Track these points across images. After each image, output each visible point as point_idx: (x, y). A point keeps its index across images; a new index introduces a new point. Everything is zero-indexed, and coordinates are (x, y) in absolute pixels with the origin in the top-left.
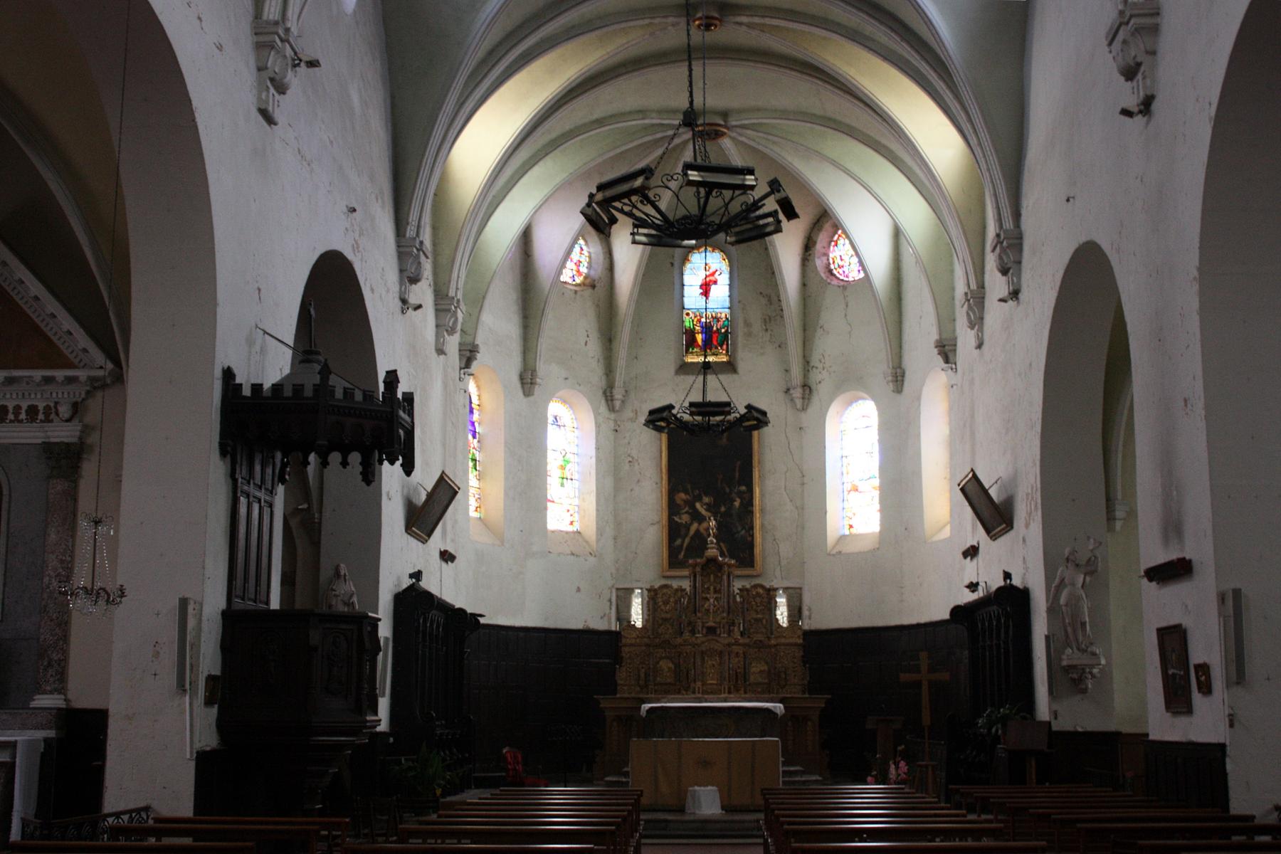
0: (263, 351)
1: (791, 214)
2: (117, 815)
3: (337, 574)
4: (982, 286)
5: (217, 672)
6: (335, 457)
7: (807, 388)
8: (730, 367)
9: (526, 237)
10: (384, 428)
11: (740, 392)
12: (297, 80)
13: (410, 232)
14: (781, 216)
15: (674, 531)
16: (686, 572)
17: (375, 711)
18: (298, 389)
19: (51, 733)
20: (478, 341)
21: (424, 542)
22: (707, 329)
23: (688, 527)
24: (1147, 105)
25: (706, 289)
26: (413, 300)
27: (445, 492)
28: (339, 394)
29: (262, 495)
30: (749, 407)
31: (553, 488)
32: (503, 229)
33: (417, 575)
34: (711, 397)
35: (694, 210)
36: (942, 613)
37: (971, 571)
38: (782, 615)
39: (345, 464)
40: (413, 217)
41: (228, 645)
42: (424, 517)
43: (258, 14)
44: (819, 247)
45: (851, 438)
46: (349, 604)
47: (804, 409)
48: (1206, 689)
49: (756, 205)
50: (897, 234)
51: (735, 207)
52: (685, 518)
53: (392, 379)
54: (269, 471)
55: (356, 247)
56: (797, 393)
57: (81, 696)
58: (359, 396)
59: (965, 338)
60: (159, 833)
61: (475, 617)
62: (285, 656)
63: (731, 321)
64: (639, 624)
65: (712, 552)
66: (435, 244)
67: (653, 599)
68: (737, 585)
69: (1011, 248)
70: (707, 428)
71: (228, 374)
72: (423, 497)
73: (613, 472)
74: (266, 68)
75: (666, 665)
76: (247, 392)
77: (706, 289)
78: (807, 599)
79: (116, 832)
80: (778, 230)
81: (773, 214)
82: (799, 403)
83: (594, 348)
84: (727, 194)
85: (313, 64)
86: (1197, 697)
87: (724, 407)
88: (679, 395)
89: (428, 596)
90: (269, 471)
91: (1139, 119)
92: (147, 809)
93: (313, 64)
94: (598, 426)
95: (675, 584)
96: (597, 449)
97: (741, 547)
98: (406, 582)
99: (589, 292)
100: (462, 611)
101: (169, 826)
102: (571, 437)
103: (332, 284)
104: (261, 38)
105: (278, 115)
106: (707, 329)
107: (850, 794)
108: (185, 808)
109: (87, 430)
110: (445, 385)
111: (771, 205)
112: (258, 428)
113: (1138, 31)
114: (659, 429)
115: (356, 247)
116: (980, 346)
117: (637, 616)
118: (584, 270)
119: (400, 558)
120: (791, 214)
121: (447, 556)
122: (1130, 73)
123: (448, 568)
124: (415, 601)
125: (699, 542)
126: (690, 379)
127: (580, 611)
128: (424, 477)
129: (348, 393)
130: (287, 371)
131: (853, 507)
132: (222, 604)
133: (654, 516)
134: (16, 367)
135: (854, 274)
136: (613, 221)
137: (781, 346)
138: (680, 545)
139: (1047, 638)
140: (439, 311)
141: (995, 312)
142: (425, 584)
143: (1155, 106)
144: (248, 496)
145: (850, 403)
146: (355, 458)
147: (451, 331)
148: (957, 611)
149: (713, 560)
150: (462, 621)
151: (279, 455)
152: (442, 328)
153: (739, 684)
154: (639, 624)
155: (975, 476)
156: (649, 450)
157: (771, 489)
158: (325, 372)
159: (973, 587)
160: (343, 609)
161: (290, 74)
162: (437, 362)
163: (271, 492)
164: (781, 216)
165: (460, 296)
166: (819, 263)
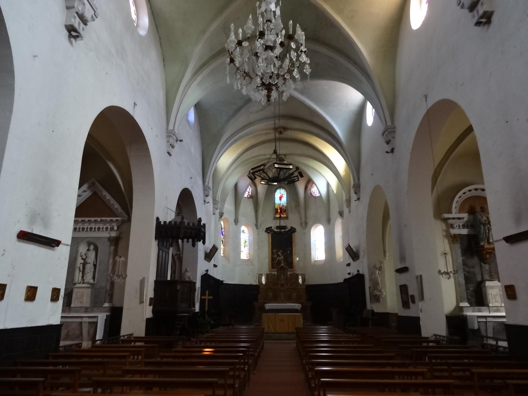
0: (167, 213)
1: (302, 176)
2: (124, 336)
3: (186, 270)
4: (350, 197)
5: (152, 296)
6: (185, 240)
7: (306, 223)
8: (287, 218)
9: (236, 186)
10: (197, 233)
11: (289, 224)
12: (177, 145)
13: (206, 184)
14: (299, 177)
15: (273, 259)
16: (276, 270)
17: (194, 307)
18: (175, 222)
19: (108, 314)
20: (224, 211)
21: (209, 262)
22: (281, 209)
23: (276, 258)
24: (392, 151)
25: (281, 198)
26: (207, 201)
27: (215, 249)
28: (186, 224)
29: (166, 250)
30: (291, 227)
31: (242, 248)
32: (230, 183)
33: (207, 271)
34: (282, 225)
35: (277, 175)
36: (341, 281)
37: (349, 270)
38: (300, 281)
39: (188, 242)
40: (207, 180)
41: (156, 290)
42: (209, 256)
43: (167, 128)
44: (309, 188)
45: (317, 235)
46: (189, 278)
47: (305, 228)
48: (414, 302)
49: (293, 174)
50: (328, 185)
51: (287, 174)
52: (275, 256)
53: (200, 220)
54: (168, 244)
55: (192, 187)
56: (304, 224)
57: (418, 274)
58: (191, 224)
59: (346, 211)
60: (135, 341)
61: (222, 281)
62: (170, 292)
63: (287, 207)
64: (264, 283)
65: (282, 265)
66: (213, 187)
67: (268, 277)
68: (289, 273)
69: (357, 188)
70: (280, 232)
71: (158, 219)
72: (209, 251)
73: (256, 244)
74: (73, 7)
75: (271, 294)
76: (162, 223)
77: (281, 198)
78: (306, 277)
79: (124, 341)
80: (298, 180)
81: (297, 176)
82: (304, 227)
83: (253, 213)
84: (285, 171)
85: (181, 141)
86: (411, 305)
87: (284, 227)
88: (273, 224)
89: (210, 276)
90: (168, 244)
91: (391, 154)
92: (132, 334)
93: (181, 141)
94: (254, 232)
95: (273, 273)
96: (254, 238)
97: (290, 264)
98: (205, 272)
99: (251, 199)
100: (219, 280)
101: (138, 339)
102: (246, 235)
103: (186, 198)
104: (169, 134)
105: (172, 153)
106: (281, 209)
107: (317, 329)
108: (142, 334)
109: (120, 233)
110: (215, 222)
111: (296, 174)
112: (166, 233)
113: (390, 132)
114: (268, 233)
115: (192, 187)
116: (350, 212)
117: (264, 281)
118: (250, 194)
119: (203, 266)
120: (302, 176)
121: (215, 266)
122: (388, 142)
123: (216, 269)
124: (206, 278)
125: (279, 262)
126: (276, 221)
127: (249, 280)
128: (209, 245)
129: (188, 224)
130: (173, 217)
131: (318, 253)
132: (155, 279)
133: (267, 256)
134: (103, 217)
135: (318, 195)
136: (256, 178)
137: (300, 213)
138: (274, 263)
139: (369, 287)
140: (214, 204)
141: (353, 204)
142: (209, 273)
143: (395, 150)
144: (162, 250)
145: (317, 227)
146: (190, 240)
147: (217, 209)
148: (345, 280)
149: (282, 267)
150: (219, 283)
151: (171, 240)
152: (215, 208)
153: (289, 299)
154: (264, 283)
155: (349, 245)
156: (266, 238)
157: (297, 248)
158: (183, 218)
159: (349, 274)
160: (188, 280)
161: (175, 143)
162: (213, 217)
163: (169, 249)
164: (299, 177)
165: (219, 200)
166: (309, 192)
